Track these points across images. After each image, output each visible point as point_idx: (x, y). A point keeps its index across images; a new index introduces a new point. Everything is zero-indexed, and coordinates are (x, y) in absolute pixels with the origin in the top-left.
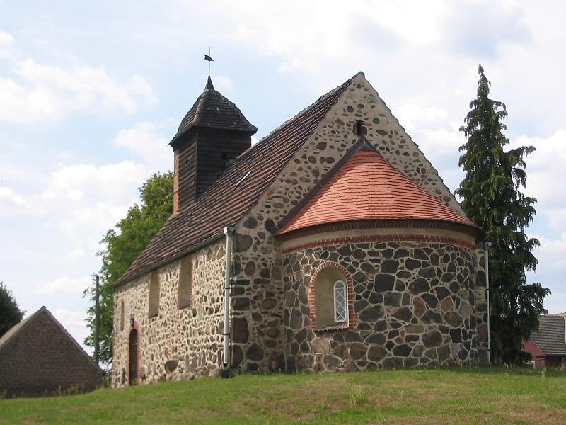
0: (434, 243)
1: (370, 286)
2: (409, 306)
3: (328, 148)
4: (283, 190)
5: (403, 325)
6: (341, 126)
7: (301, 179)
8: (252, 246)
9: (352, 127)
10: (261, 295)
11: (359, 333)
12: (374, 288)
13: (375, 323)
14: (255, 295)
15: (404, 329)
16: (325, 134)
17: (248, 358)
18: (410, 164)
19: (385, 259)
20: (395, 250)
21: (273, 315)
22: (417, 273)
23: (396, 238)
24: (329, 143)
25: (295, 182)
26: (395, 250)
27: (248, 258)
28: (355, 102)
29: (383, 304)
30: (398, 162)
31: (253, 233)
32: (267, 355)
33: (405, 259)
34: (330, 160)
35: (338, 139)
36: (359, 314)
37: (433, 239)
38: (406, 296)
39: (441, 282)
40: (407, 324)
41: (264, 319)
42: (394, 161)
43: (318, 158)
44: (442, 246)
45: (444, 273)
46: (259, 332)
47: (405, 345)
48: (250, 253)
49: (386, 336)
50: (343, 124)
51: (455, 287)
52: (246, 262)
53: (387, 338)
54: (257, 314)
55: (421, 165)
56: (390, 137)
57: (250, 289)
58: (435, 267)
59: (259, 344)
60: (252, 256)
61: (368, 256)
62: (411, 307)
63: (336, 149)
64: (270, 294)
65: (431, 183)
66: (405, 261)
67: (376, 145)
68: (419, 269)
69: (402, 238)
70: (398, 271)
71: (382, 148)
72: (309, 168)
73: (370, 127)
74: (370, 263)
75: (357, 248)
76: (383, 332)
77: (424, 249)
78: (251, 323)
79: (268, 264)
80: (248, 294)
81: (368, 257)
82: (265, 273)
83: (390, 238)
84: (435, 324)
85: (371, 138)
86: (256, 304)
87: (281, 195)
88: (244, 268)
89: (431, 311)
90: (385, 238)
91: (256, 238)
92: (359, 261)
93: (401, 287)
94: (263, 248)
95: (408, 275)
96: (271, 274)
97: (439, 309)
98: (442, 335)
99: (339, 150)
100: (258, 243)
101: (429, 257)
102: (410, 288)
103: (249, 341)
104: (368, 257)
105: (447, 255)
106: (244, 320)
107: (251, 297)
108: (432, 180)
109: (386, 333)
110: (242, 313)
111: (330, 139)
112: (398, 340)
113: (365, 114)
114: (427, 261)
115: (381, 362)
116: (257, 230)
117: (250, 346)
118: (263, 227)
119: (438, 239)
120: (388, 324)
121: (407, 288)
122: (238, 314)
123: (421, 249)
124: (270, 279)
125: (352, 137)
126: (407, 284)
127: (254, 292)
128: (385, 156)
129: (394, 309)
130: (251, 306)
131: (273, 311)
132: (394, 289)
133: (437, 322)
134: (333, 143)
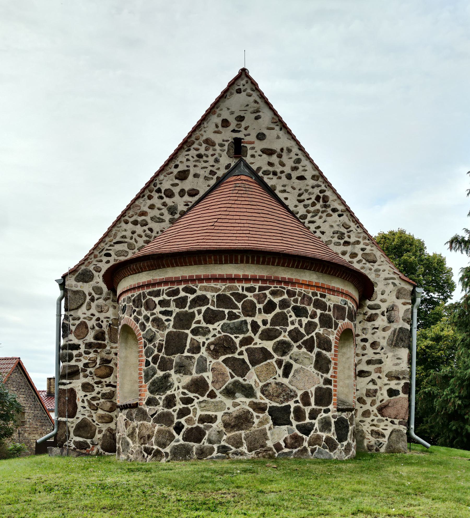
0: (248, 285)
1: (160, 351)
2: (205, 375)
3: (191, 177)
4: (128, 234)
5: (196, 401)
6: (211, 148)
7: (152, 219)
8: (86, 304)
9: (226, 148)
10: (94, 361)
11: (148, 410)
12: (163, 350)
13: (163, 397)
14: (87, 361)
15: (197, 406)
16: (188, 160)
17: (76, 436)
18: (306, 191)
19: (178, 310)
20: (191, 297)
21: (107, 386)
22: (219, 329)
23: (192, 280)
24: (193, 171)
25: (144, 224)
26: (191, 297)
27: (79, 319)
28: (232, 113)
29: (172, 372)
30: (288, 189)
31: (87, 288)
32: (100, 432)
33: (204, 309)
34: (193, 193)
35: (205, 165)
36: (148, 384)
37: (246, 279)
38: (203, 360)
39: (256, 339)
40: (201, 399)
41: (97, 389)
42: (283, 188)
43: (176, 190)
44: (261, 289)
45: (262, 327)
46: (90, 405)
47: (197, 428)
48: (82, 313)
49: (175, 414)
50: (213, 144)
51: (283, 348)
52: (77, 322)
53: (175, 416)
54: (88, 384)
55: (322, 191)
56: (280, 156)
57: (80, 355)
58: (249, 320)
59: (90, 419)
60: (85, 316)
61: (158, 306)
62: (208, 376)
63: (201, 179)
64: (106, 361)
65: (335, 215)
66: (203, 312)
67: (259, 169)
68: (222, 323)
69: (200, 280)
70: (194, 326)
71: (266, 173)
72: (164, 204)
73: (252, 145)
74: (161, 316)
75: (148, 297)
76: (171, 410)
77: (231, 294)
78: (80, 394)
79: (104, 325)
80: (77, 361)
81: (159, 309)
82: (100, 336)
83: (185, 280)
84: (244, 399)
85: (252, 160)
86: (88, 373)
87: (126, 240)
88: (73, 330)
89: (237, 381)
90: (179, 281)
91: (90, 294)
92: (149, 315)
93: (196, 349)
94: (98, 306)
95: (205, 332)
96: (107, 336)
97: (252, 378)
98: (255, 414)
99: (206, 178)
100: (92, 300)
101: (240, 305)
102: (208, 349)
103: (77, 416)
104: (159, 309)
105: (270, 302)
106: (72, 392)
107: (81, 365)
108: (338, 211)
109: (174, 411)
110: (70, 383)
111: (195, 166)
112: (188, 421)
113: (246, 129)
114: (234, 311)
115: (168, 449)
116: (93, 283)
117: (79, 421)
118: (100, 280)
119: (255, 280)
120: (178, 399)
121: (203, 349)
122: (64, 384)
123: (228, 294)
124: (106, 342)
125: (225, 160)
126: (204, 343)
127: (85, 358)
128: (270, 183)
129: (187, 379)
130: (81, 374)
131: (108, 380)
132: (186, 351)
133: (247, 396)
134: (198, 171)
